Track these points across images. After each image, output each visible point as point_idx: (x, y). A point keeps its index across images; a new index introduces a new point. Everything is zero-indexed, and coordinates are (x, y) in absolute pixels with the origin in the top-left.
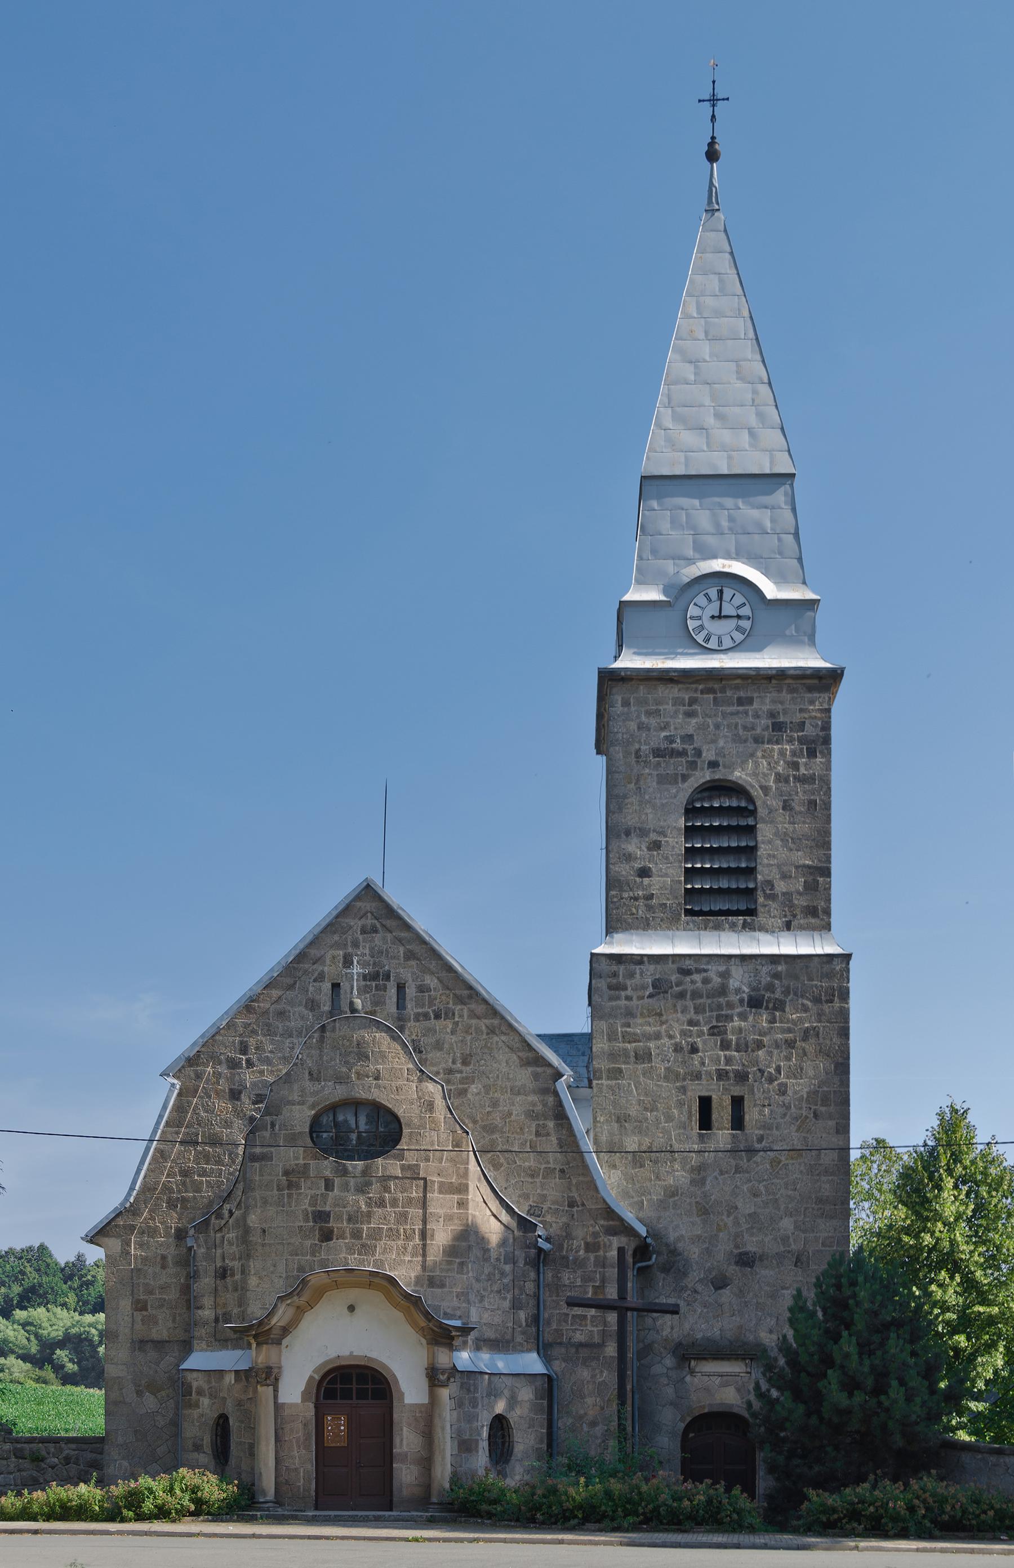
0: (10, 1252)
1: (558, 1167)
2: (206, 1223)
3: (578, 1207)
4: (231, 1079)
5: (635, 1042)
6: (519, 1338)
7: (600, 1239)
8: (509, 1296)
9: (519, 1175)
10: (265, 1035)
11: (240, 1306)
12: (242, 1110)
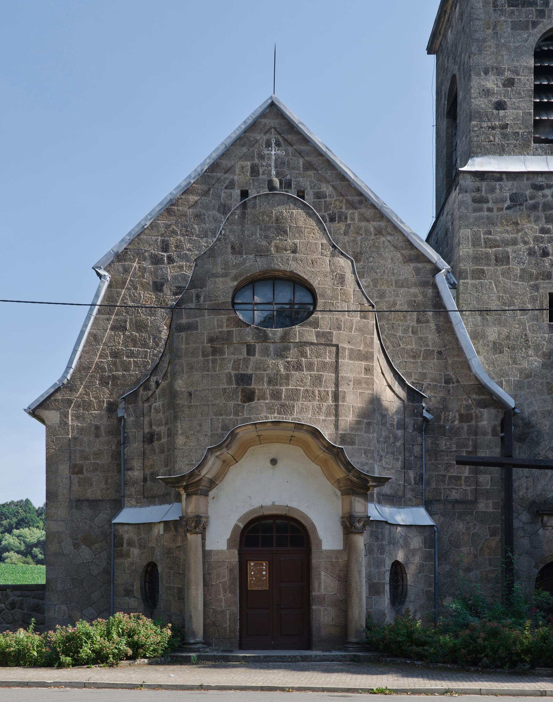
0: (12, 503)
1: (436, 350)
2: (136, 394)
3: (453, 383)
4: (154, 274)
5: (495, 247)
6: (409, 495)
7: (472, 411)
8: (401, 458)
9: (403, 357)
10: (183, 235)
11: (167, 465)
12: (164, 301)
